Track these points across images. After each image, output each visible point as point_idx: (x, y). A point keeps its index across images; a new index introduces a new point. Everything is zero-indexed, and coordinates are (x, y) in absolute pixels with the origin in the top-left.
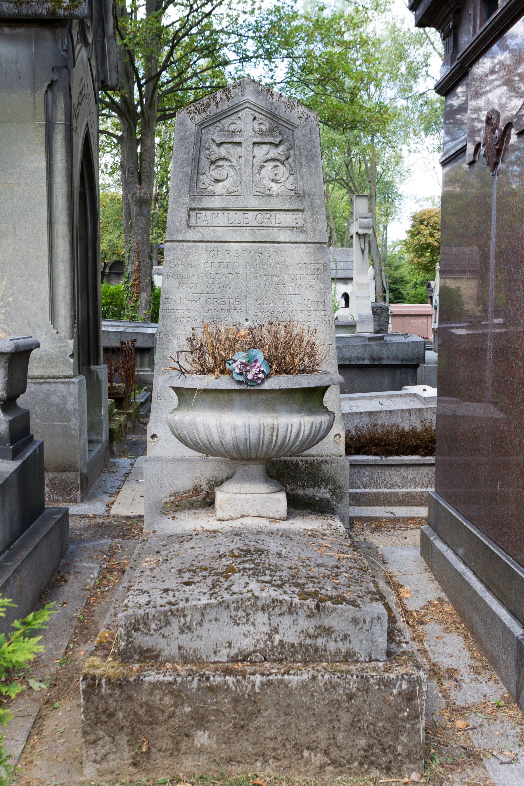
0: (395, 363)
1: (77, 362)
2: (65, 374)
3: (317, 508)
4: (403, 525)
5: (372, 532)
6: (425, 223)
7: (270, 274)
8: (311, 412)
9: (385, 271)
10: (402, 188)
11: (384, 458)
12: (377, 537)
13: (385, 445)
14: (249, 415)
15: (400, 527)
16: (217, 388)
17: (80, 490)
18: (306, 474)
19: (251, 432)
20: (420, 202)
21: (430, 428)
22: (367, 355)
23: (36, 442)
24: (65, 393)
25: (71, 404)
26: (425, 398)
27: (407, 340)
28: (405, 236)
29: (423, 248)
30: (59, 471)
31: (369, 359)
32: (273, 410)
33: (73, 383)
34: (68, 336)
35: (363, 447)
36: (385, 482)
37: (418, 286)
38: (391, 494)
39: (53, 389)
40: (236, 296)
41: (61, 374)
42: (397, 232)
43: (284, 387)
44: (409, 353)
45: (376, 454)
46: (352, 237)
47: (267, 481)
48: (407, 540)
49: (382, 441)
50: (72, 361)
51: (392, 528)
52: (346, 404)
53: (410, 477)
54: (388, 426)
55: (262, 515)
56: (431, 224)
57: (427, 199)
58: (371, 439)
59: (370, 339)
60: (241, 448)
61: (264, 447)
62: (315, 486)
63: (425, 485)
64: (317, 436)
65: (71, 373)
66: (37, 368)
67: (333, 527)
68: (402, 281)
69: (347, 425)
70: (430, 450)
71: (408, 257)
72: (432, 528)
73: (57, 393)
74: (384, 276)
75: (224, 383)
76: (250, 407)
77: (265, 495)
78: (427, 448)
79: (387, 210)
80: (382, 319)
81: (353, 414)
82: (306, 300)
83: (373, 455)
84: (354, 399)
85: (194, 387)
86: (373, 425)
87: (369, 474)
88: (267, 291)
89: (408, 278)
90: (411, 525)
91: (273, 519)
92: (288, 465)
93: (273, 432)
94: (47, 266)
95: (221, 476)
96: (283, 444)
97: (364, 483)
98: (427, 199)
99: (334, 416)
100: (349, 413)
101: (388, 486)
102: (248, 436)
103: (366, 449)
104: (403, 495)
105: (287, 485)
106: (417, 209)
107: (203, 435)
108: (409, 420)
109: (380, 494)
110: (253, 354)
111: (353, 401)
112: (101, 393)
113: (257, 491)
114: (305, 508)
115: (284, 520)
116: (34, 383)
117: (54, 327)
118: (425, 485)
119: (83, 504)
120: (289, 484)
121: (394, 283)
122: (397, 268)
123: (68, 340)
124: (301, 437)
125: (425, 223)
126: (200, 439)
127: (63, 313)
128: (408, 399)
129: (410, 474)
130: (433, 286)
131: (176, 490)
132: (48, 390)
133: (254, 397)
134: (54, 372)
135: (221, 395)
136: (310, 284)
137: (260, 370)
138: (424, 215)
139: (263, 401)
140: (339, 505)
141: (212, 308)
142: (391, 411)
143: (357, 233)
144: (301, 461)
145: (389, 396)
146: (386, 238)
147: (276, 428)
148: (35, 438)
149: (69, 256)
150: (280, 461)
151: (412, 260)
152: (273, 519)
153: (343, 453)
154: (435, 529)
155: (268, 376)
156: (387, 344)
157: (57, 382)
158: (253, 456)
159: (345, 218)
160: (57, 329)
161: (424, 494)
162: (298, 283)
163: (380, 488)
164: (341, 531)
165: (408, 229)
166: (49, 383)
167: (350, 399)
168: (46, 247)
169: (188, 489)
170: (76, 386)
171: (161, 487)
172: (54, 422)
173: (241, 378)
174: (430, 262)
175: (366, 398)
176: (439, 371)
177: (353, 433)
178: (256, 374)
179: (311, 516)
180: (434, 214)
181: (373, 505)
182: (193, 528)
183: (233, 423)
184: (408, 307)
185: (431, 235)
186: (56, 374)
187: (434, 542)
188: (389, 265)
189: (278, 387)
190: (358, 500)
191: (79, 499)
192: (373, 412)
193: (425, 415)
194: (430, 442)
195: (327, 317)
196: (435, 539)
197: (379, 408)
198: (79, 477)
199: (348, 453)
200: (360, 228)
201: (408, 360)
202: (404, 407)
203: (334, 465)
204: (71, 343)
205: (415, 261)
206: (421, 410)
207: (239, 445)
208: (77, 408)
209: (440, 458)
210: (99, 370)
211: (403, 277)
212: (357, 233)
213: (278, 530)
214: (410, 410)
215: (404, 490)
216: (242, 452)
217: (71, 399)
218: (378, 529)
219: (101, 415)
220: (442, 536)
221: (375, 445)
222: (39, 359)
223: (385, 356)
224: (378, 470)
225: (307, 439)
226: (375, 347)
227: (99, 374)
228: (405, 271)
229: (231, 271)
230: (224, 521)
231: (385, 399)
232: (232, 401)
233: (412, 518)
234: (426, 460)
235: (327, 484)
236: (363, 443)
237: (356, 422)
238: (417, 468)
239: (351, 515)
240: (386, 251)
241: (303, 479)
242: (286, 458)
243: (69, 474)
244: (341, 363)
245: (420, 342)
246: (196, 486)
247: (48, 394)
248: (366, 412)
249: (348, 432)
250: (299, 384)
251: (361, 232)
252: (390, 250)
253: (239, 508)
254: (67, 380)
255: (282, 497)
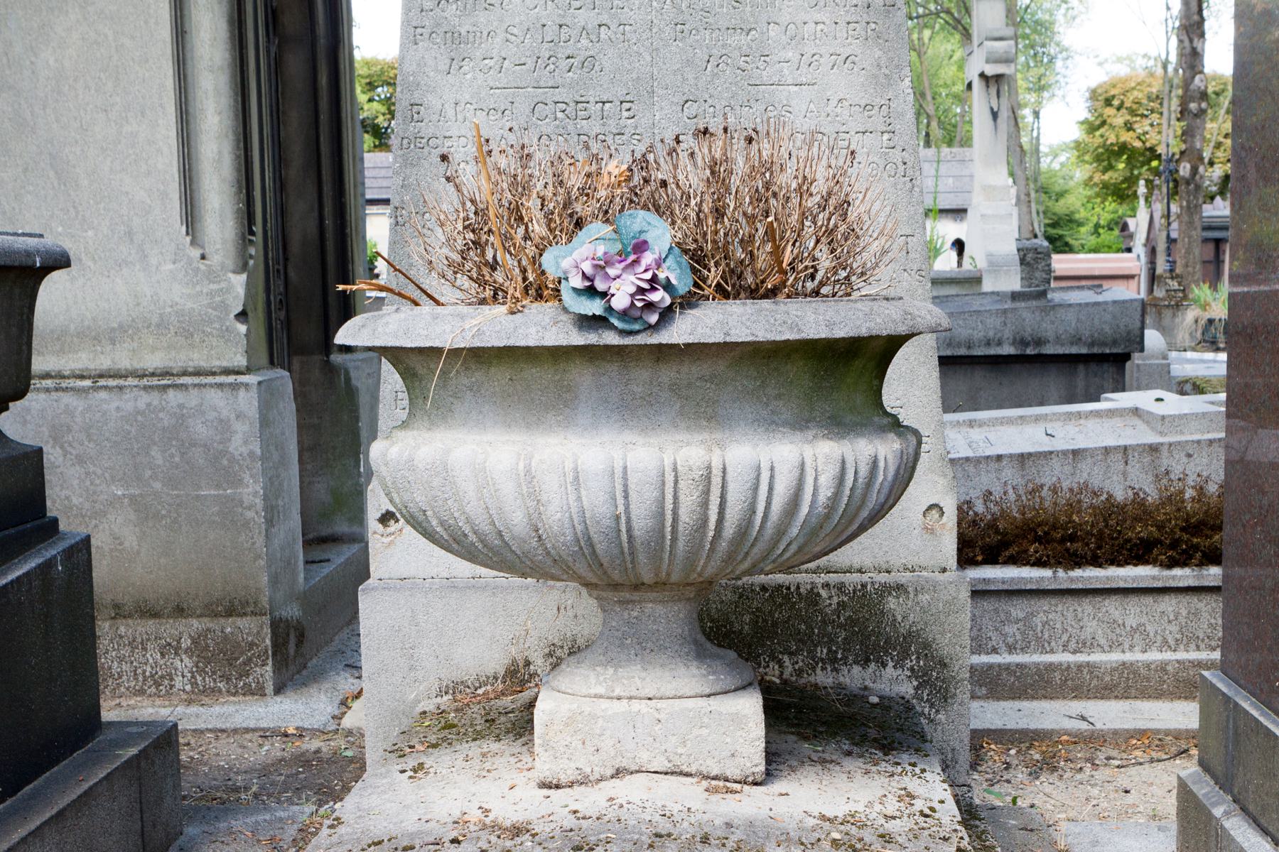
0: (1074, 350)
1: (262, 332)
2: (225, 364)
3: (873, 733)
4: (1114, 753)
5: (1034, 775)
6: (1116, 102)
7: (723, 23)
8: (838, 425)
9: (1038, 202)
10: (1067, 35)
11: (1061, 573)
12: (1048, 789)
13: (1063, 541)
14: (629, 436)
15: (1108, 758)
16: (511, 342)
17: (270, 662)
18: (840, 626)
19: (633, 496)
20: (1106, 65)
21: (1182, 492)
22: (1007, 334)
23: (64, 536)
24: (225, 413)
25: (243, 441)
26: (1163, 417)
27: (1100, 298)
28: (1076, 133)
29: (1113, 151)
30: (216, 615)
31: (1014, 343)
32: (709, 420)
33: (247, 385)
34: (230, 263)
35: (1005, 544)
36: (1065, 637)
37: (1101, 231)
38: (1080, 667)
39: (194, 403)
40: (621, 92)
41: (216, 364)
42: (1059, 124)
43: (740, 335)
44: (1107, 329)
45: (1039, 563)
46: (969, 86)
47: (701, 656)
48: (1130, 799)
49: (1054, 527)
50: (243, 328)
51: (1087, 760)
52: (959, 436)
53: (1131, 621)
54: (1071, 490)
55: (685, 769)
56: (1127, 104)
57: (1119, 60)
58: (1026, 522)
59: (1015, 296)
60: (600, 548)
61: (681, 544)
62: (867, 661)
63: (1172, 643)
64: (860, 508)
65: (241, 361)
66: (154, 349)
67: (919, 805)
68: (1071, 221)
69: (963, 490)
70: (1184, 551)
71: (1080, 174)
72: (1213, 776)
73: (203, 413)
74: (1034, 211)
75: (540, 327)
76: (633, 411)
77: (691, 703)
78: (1174, 544)
79: (1040, 79)
80: (1038, 274)
81: (977, 461)
82: (833, 102)
83: (1033, 565)
84: (981, 424)
85: (440, 345)
86: (1031, 486)
87: (1021, 615)
88: (715, 75)
89: (1081, 214)
90: (1138, 753)
91: (720, 783)
92: (787, 598)
93: (707, 492)
94: (169, 82)
95: (586, 632)
96: (743, 531)
97: (1010, 640)
98: (1119, 60)
99: (919, 443)
100: (967, 459)
101: (1072, 645)
102: (621, 509)
103: (1013, 550)
104: (1116, 669)
105: (786, 658)
106: (1097, 77)
107: (474, 509)
108: (1125, 474)
109: (1051, 667)
110: (636, 228)
111: (977, 430)
112: (357, 419)
113: (669, 688)
114: (834, 735)
115: (756, 784)
116: (145, 388)
117: (193, 243)
118: (1172, 643)
119: (278, 699)
120: (791, 654)
121: (1054, 225)
122: (1061, 195)
123: (231, 275)
124: (804, 510)
125: (1116, 102)
126: (468, 520)
127: (217, 206)
128: (1117, 422)
129: (1131, 613)
130: (1132, 227)
131: (457, 676)
132: (181, 406)
133: (642, 374)
134: (198, 359)
135: (532, 373)
136: (848, 51)
137: (654, 279)
138: (1114, 86)
139: (674, 388)
140: (941, 717)
141: (549, 130)
142: (1075, 452)
143: (982, 75)
144: (826, 585)
145: (1069, 416)
146: (1038, 138)
147: (716, 481)
148: (62, 527)
149: (227, 55)
150: (764, 588)
151: (1091, 178)
152: (720, 783)
153: (952, 562)
154: (1225, 783)
155: (688, 301)
156: (1053, 307)
157: (205, 385)
158: (648, 577)
159: (956, 96)
160: (203, 247)
161: (1169, 668)
162: (809, 50)
163: (1052, 651)
164: (946, 820)
165: (1082, 119)
166: (183, 387)
167: (971, 424)
168: (165, 32)
169: (490, 672)
170: (254, 393)
171: (411, 668)
172: (200, 488)
173: (594, 307)
174: (1126, 180)
175: (1010, 421)
176: (1226, 324)
177: (980, 507)
178: (641, 291)
179: (850, 764)
180: (1133, 85)
181: (1033, 698)
182: (456, 814)
183: (569, 465)
184: (1088, 261)
185: (1129, 127)
186: (203, 364)
187: (1227, 824)
188: (1044, 190)
189: (719, 338)
190: (995, 684)
191: (270, 688)
192: (1030, 454)
193: (1165, 462)
194: (1183, 529)
195: (897, 152)
196: (1227, 813)
197: (1046, 445)
198: (267, 631)
199: (965, 560)
200: (987, 61)
201: (1104, 344)
202: (1111, 442)
203: (924, 598)
204: (239, 282)
205: (1096, 179)
206: (1154, 449)
207: (596, 538)
208: (258, 452)
209: (1238, 571)
210: (350, 365)
211: (1073, 213)
212: (982, 75)
213: (729, 825)
214: (1126, 448)
215: (1115, 657)
216: (605, 561)
217: (241, 428)
218: (1049, 765)
219: (359, 474)
220: (1251, 808)
221: (1038, 539)
222: (158, 326)
223: (1050, 335)
224: (1044, 604)
225: (828, 516)
226: (1027, 315)
227: (353, 374)
228: (1074, 202)
229: (604, 18)
230: (558, 787)
231: (1059, 424)
232: (569, 389)
233: (1141, 734)
234: (1174, 577)
235: (905, 654)
236: (1005, 534)
237: (987, 480)
238: (1148, 600)
239: (976, 724)
240: (1038, 162)
241: (831, 641)
242: (780, 578)
243: (243, 623)
244: (949, 353)
245: (1132, 301)
246: (514, 661)
247: (181, 418)
248: (1011, 456)
249: (964, 510)
250: (794, 326)
251: (991, 70)
252: (1045, 163)
253: (607, 744)
254: (231, 379)
255: (750, 706)
